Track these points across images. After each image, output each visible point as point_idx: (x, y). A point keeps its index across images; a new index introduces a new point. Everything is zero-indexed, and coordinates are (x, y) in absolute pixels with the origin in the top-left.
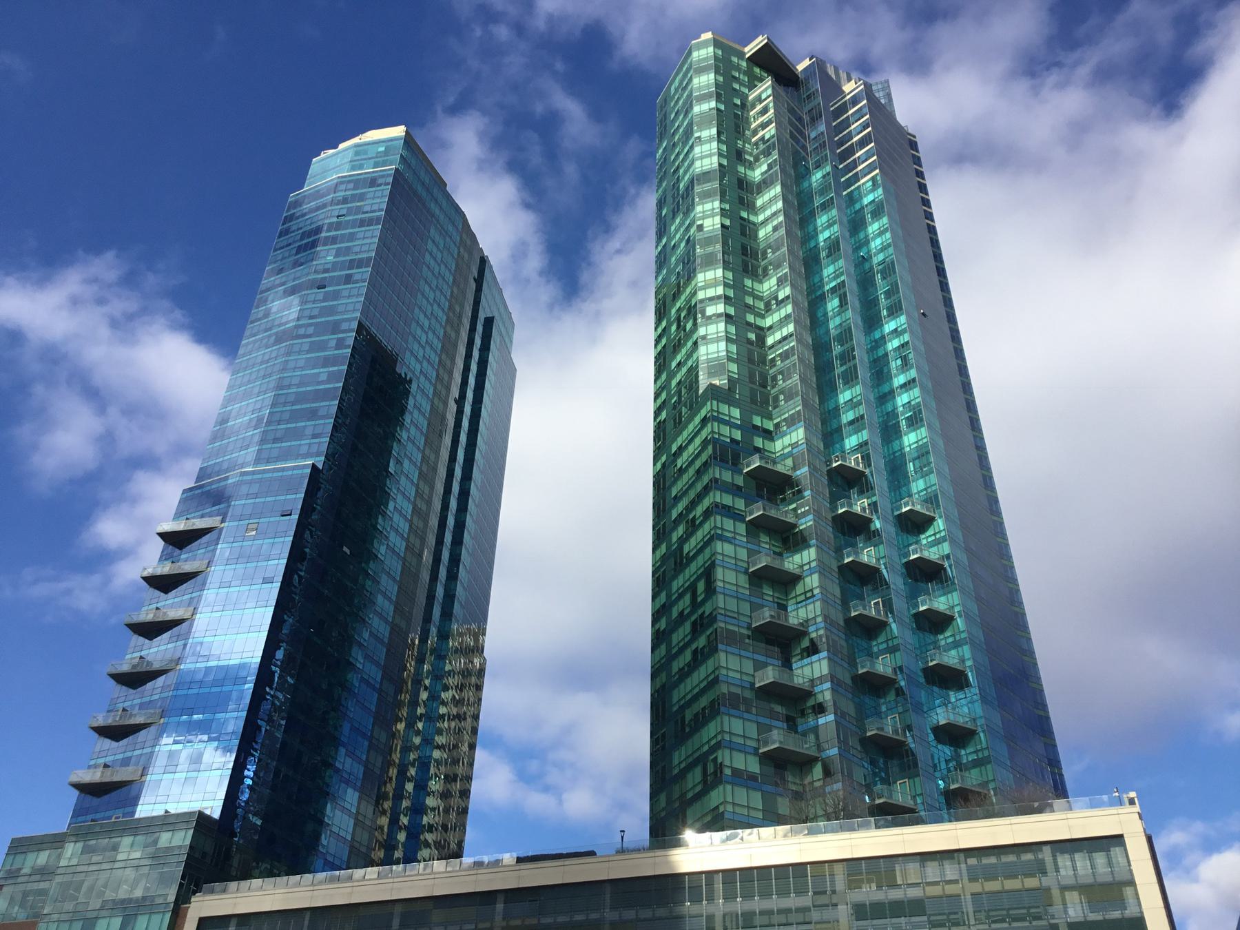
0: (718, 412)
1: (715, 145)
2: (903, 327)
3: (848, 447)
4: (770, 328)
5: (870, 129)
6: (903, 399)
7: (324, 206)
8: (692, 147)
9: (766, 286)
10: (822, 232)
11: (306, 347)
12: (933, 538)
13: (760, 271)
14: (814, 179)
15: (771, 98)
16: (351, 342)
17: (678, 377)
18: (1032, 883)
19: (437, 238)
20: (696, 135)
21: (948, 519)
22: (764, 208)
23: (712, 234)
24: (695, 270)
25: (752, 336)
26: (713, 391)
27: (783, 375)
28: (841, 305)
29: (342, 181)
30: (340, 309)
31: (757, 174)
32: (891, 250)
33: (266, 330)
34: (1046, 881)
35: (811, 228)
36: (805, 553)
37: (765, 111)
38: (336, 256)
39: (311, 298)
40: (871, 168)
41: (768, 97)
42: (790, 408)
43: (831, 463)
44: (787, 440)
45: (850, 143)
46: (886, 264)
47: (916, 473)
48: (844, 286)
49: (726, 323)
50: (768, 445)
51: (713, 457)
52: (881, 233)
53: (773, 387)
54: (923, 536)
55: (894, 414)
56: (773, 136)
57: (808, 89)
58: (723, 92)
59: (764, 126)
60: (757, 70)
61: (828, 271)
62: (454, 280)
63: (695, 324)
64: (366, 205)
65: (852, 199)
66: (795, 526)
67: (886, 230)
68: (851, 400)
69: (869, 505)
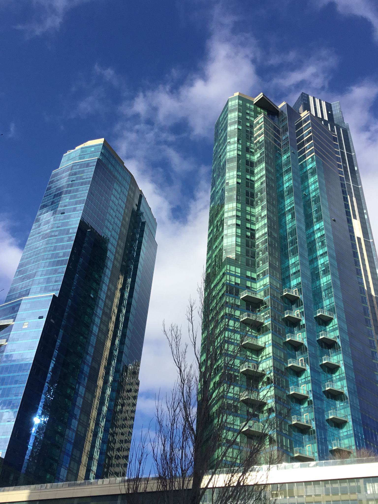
0: (230, 270)
1: (236, 145)
2: (322, 227)
3: (292, 285)
4: (258, 229)
5: (311, 134)
6: (321, 261)
8: (226, 146)
9: (257, 210)
10: (286, 183)
12: (332, 328)
13: (255, 203)
14: (283, 159)
15: (263, 123)
16: (74, 238)
17: (216, 253)
18: (353, 497)
19: (117, 188)
20: (228, 141)
21: (339, 318)
22: (258, 173)
23: (232, 187)
24: (224, 204)
25: (249, 234)
26: (229, 261)
27: (262, 252)
28: (292, 218)
31: (255, 158)
32: (318, 191)
33: (38, 233)
34: (360, 496)
35: (281, 182)
36: (267, 336)
37: (260, 128)
38: (70, 199)
39: (58, 218)
40: (311, 152)
41: (262, 122)
42: (264, 267)
43: (283, 293)
44: (262, 283)
45: (302, 141)
46: (316, 197)
47: (325, 297)
48: (294, 209)
49: (236, 228)
50: (254, 285)
51: (227, 291)
52: (315, 183)
53: (257, 258)
54: (327, 327)
55: (317, 268)
56: (263, 141)
57: (282, 117)
58: (241, 121)
59: (259, 135)
60: (259, 109)
61: (287, 202)
62: (126, 206)
63: (223, 229)
64: (84, 175)
65: (302, 167)
66: (263, 323)
67: (316, 181)
68: (294, 263)
69: (300, 313)
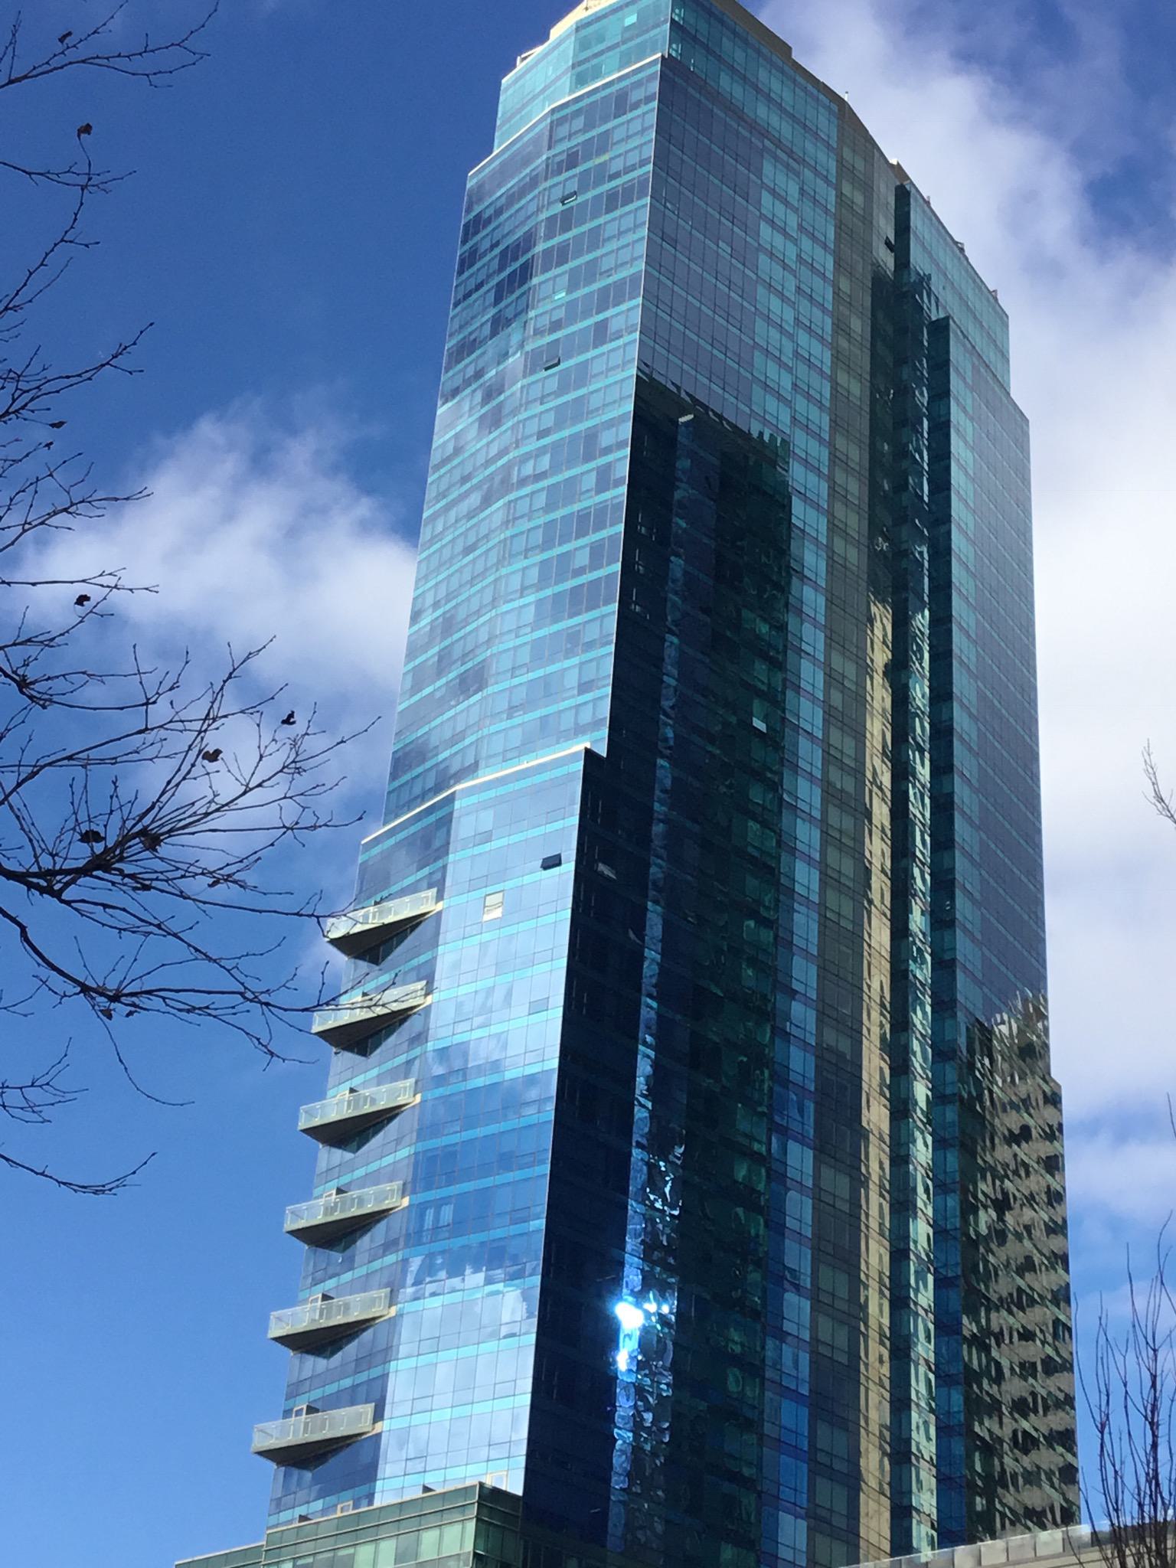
7: (534, 181)
11: (541, 500)
16: (624, 470)
29: (560, 118)
30: (606, 264)
62: (838, 264)
